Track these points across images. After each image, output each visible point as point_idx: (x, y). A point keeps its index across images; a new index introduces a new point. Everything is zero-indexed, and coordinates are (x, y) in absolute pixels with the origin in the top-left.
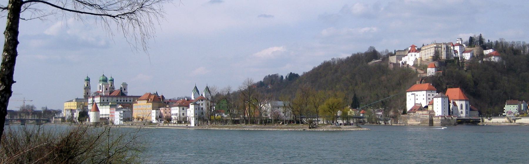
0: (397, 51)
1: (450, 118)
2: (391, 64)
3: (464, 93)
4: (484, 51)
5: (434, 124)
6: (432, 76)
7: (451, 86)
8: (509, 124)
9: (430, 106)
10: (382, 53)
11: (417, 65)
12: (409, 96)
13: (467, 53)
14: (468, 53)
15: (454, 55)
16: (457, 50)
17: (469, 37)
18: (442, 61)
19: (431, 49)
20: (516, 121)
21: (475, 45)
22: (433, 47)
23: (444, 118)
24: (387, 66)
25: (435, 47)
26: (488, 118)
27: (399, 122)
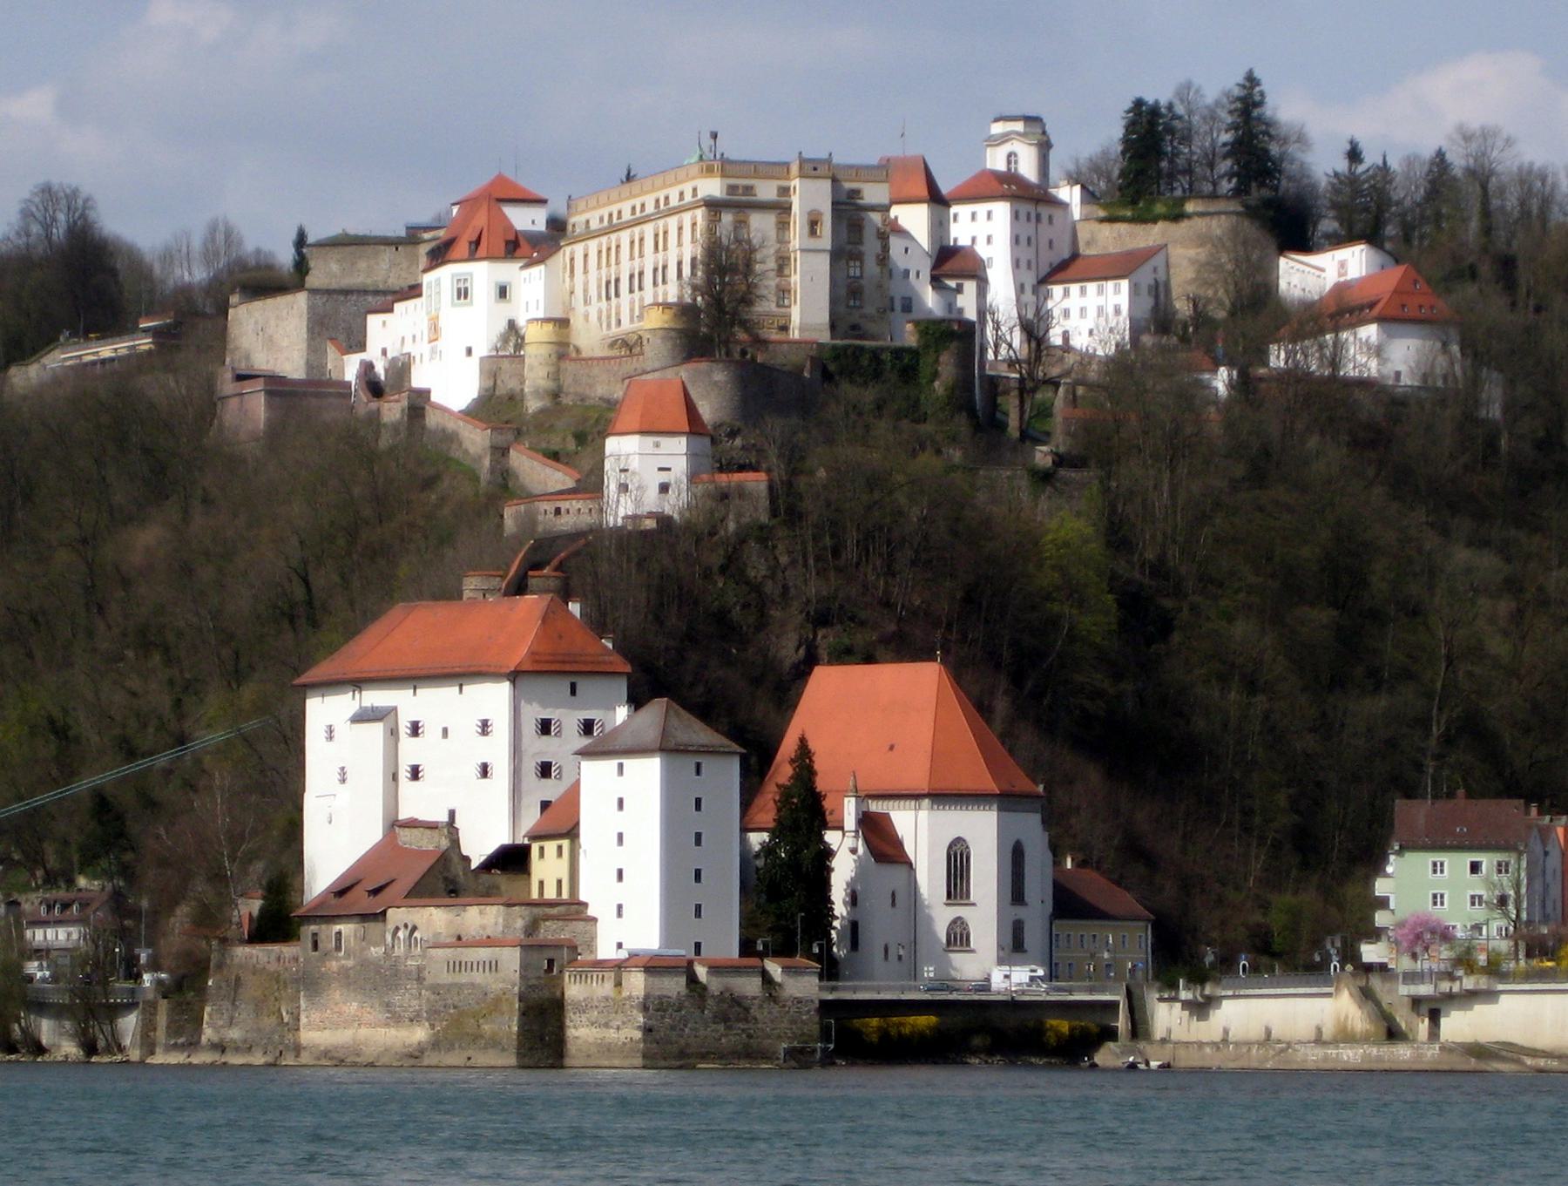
0: (321, 245)
1: (750, 986)
2: (248, 387)
3: (1006, 737)
4: (1283, 262)
5: (572, 1048)
6: (650, 524)
7: (861, 638)
8: (1374, 1051)
9: (550, 847)
10: (168, 257)
11: (514, 399)
12: (330, 733)
13: (1092, 287)
14: (1110, 284)
15: (930, 300)
16: (982, 250)
17: (1128, 105)
18: (781, 358)
19: (672, 222)
20: (1443, 1021)
21: (1192, 193)
22: (688, 198)
23: (674, 986)
24: (210, 405)
25: (713, 206)
26: (1185, 995)
27: (208, 1034)
